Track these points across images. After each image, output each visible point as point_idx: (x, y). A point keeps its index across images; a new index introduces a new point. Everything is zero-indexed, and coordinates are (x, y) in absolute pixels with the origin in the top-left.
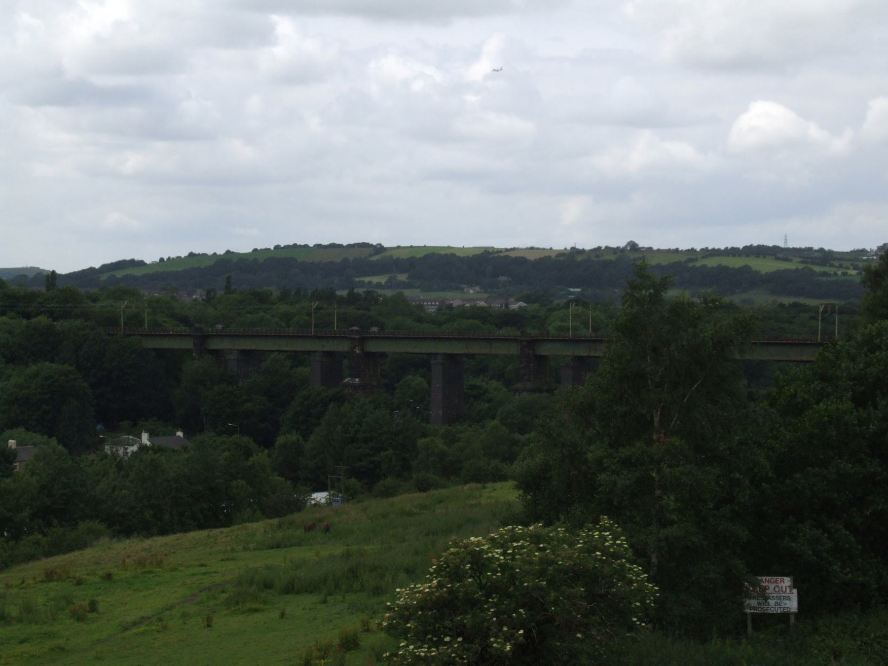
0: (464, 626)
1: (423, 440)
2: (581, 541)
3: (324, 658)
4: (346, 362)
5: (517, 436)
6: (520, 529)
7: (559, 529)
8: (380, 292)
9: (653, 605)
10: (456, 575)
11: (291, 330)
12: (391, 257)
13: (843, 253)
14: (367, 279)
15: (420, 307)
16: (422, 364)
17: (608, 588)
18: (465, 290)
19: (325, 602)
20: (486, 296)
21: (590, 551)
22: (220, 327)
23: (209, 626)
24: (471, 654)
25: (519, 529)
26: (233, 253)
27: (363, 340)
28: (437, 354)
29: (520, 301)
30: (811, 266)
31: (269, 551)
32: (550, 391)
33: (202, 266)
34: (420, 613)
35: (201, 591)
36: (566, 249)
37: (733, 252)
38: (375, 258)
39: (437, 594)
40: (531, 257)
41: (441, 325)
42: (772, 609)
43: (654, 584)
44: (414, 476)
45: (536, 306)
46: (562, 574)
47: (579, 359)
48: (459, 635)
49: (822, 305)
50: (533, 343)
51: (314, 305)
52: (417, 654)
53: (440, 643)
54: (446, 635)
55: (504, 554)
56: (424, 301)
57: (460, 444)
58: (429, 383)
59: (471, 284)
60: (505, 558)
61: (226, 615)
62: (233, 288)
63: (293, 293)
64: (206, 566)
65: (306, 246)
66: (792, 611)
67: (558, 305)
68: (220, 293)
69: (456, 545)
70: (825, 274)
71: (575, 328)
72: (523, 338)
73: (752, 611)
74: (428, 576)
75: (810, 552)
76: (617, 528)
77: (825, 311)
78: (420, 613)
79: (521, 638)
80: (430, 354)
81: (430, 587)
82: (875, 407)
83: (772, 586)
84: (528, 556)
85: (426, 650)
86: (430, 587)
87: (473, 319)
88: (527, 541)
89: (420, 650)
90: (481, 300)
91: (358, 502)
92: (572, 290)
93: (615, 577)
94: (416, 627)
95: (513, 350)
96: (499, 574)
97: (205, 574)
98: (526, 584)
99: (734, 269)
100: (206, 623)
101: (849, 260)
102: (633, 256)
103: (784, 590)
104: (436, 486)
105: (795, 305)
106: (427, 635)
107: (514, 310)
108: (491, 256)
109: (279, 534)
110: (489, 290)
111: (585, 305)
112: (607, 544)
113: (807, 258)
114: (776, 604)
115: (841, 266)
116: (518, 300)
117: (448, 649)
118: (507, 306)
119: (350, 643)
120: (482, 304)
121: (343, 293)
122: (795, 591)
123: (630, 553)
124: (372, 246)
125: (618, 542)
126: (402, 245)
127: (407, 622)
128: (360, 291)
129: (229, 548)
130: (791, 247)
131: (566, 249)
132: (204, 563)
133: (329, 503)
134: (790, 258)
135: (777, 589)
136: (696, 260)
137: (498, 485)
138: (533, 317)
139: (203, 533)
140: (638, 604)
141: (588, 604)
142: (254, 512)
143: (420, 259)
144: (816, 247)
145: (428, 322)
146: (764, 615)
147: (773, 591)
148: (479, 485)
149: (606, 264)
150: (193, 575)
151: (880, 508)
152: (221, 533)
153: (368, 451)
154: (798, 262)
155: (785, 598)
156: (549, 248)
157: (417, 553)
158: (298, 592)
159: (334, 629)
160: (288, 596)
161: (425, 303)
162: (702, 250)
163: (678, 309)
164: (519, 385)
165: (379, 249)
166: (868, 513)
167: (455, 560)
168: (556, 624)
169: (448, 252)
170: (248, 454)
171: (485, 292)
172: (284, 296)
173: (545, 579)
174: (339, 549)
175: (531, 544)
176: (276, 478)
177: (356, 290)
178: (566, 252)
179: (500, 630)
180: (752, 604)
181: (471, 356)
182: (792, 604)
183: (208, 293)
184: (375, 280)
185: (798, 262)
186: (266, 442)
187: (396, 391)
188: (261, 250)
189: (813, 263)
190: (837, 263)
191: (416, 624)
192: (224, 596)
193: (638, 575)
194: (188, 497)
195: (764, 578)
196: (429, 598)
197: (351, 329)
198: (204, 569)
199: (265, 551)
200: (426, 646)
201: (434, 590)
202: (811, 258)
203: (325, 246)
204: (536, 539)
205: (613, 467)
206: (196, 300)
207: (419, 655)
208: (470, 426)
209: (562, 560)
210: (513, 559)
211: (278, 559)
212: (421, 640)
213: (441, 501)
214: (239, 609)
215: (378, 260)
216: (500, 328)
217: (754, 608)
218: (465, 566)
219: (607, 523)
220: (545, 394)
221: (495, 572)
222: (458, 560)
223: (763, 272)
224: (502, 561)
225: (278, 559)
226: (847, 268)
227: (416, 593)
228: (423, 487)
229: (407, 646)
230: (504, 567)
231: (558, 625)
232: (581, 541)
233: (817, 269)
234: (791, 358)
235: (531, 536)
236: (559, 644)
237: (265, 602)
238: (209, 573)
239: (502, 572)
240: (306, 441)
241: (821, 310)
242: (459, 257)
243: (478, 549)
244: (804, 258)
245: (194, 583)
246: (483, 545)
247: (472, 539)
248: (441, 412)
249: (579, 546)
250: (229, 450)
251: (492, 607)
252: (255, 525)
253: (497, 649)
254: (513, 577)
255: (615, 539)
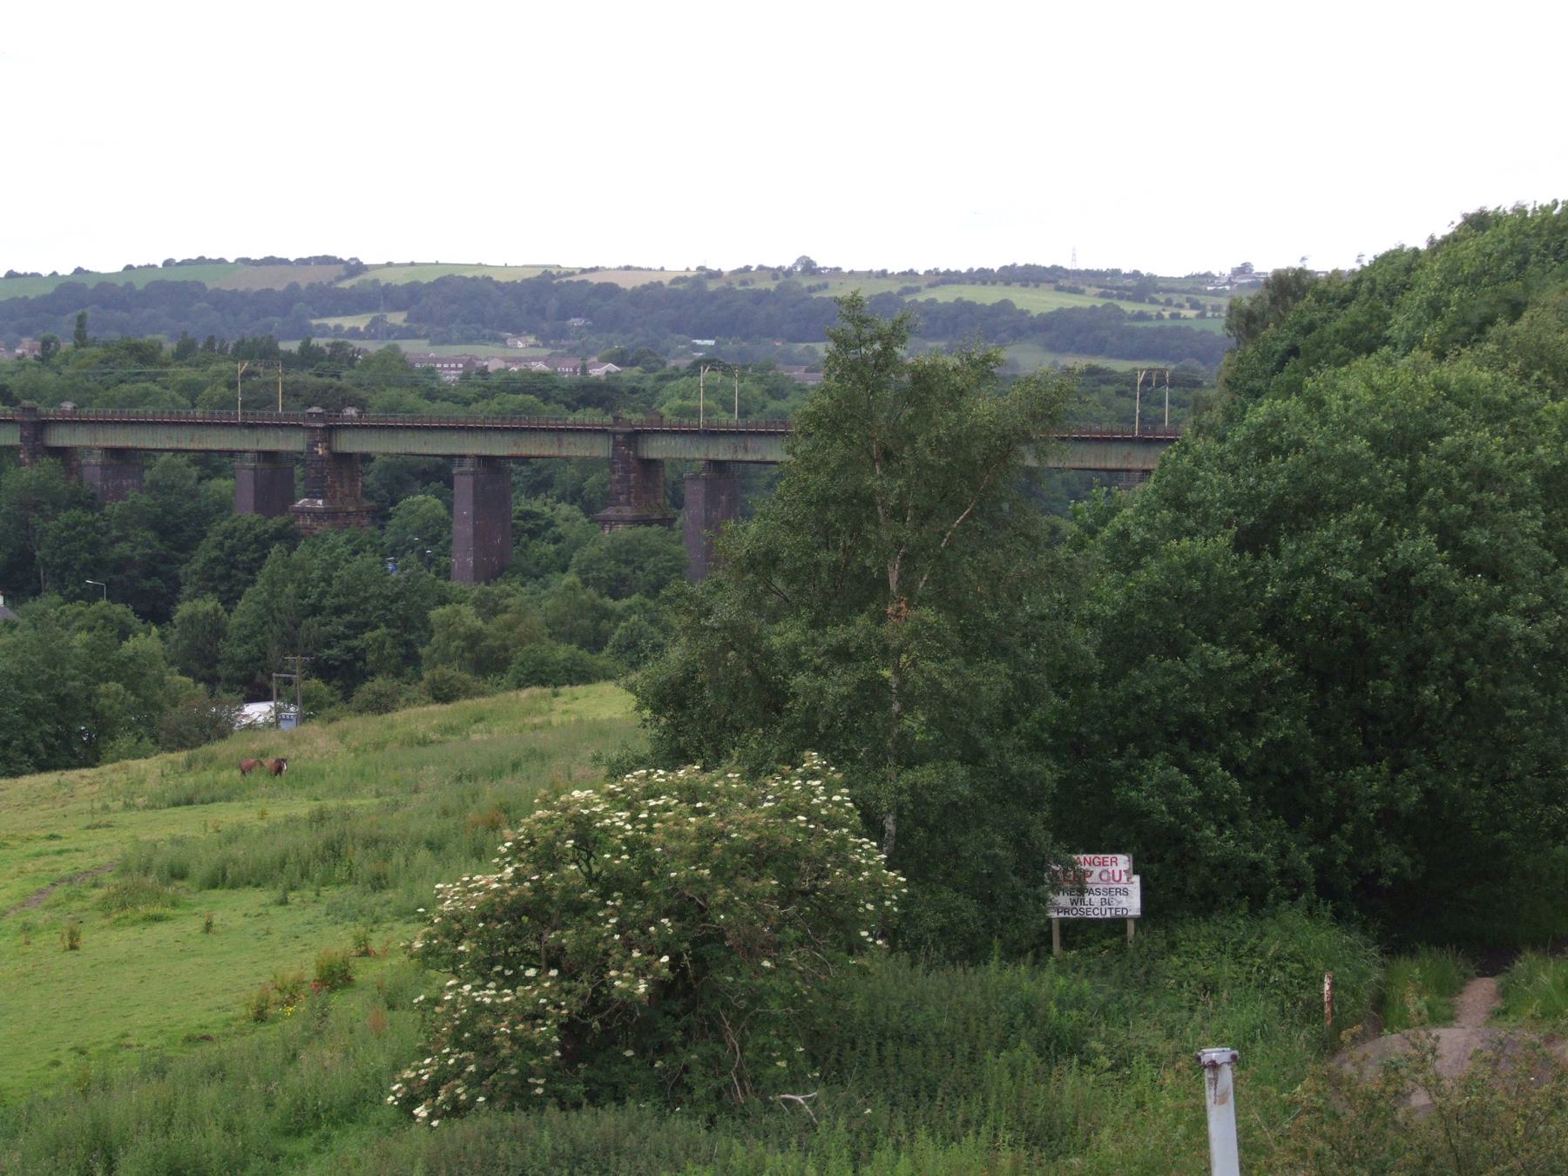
0: (562, 949)
1: (440, 610)
2: (770, 797)
3: (289, 1005)
4: (299, 471)
5: (609, 602)
6: (660, 776)
7: (730, 775)
8: (358, 344)
9: (895, 909)
10: (549, 858)
11: (199, 412)
12: (376, 281)
13: (1172, 279)
14: (332, 322)
15: (430, 371)
16: (438, 473)
17: (816, 879)
18: (509, 343)
19: (283, 902)
20: (546, 352)
21: (787, 814)
22: (68, 406)
23: (73, 947)
24: (574, 1000)
25: (659, 776)
26: (88, 272)
27: (331, 430)
28: (463, 457)
29: (608, 362)
30: (1116, 302)
31: (173, 810)
32: (667, 522)
33: (32, 296)
34: (481, 925)
35: (54, 885)
36: (688, 270)
37: (982, 277)
38: (346, 284)
39: (513, 893)
40: (627, 283)
41: (467, 404)
42: (1096, 911)
43: (898, 872)
44: (426, 675)
45: (636, 371)
46: (738, 856)
47: (717, 465)
48: (551, 965)
49: (1142, 371)
50: (635, 436)
51: (242, 368)
52: (478, 999)
53: (515, 981)
54: (528, 966)
55: (633, 820)
56: (437, 360)
57: (507, 616)
58: (449, 507)
59: (518, 331)
60: (634, 827)
61: (103, 927)
62: (90, 334)
63: (200, 346)
64: (60, 838)
65: (221, 261)
66: (1130, 913)
67: (676, 369)
68: (67, 345)
69: (546, 804)
70: (1141, 316)
71: (708, 412)
72: (617, 428)
73: (1062, 915)
74: (497, 860)
75: (1164, 808)
76: (834, 772)
77: (1146, 382)
78: (481, 925)
79: (665, 971)
80: (451, 457)
81: (500, 881)
82: (1276, 554)
83: (1097, 870)
84: (675, 824)
85: (493, 992)
86: (500, 881)
87: (525, 393)
88: (674, 798)
89: (481, 993)
90: (537, 359)
91: (332, 720)
92: (699, 342)
93: (830, 859)
94: (474, 951)
95: (601, 449)
96: (625, 857)
97: (60, 853)
98: (673, 874)
99: (983, 306)
100: (67, 944)
101: (1183, 292)
102: (807, 282)
103: (1117, 878)
104: (468, 693)
105: (1092, 371)
106: (493, 965)
107: (598, 378)
108: (555, 282)
109: (189, 780)
110: (552, 342)
111: (727, 370)
112: (815, 801)
113: (1111, 288)
114: (1103, 902)
115: (1169, 303)
116: (605, 360)
117: (533, 990)
118: (584, 370)
119: (335, 978)
120: (540, 366)
121: (293, 346)
122: (1136, 879)
123: (856, 818)
124: (341, 261)
125: (836, 798)
126: (396, 261)
127: (458, 943)
128: (320, 342)
129: (98, 805)
130: (1083, 268)
131: (688, 270)
132: (56, 832)
133: (275, 724)
134: (1081, 287)
135: (1105, 876)
136: (918, 290)
137: (580, 690)
138: (633, 391)
139: (50, 778)
140: (870, 907)
141: (781, 908)
142: (140, 740)
143: (429, 285)
144: (1126, 270)
145: (444, 400)
146: (1080, 921)
147: (1098, 880)
148: (548, 690)
149: (760, 297)
150: (39, 855)
151: (1280, 735)
152: (83, 777)
153: (341, 628)
154: (1095, 295)
155: (1118, 891)
156: (658, 267)
157: (446, 813)
158: (234, 886)
159: (302, 951)
160: (216, 893)
161: (439, 366)
162: (928, 272)
163: (924, 380)
164: (609, 512)
165: (355, 268)
166: (1260, 745)
167: (546, 831)
168: (727, 944)
169: (479, 274)
170: (124, 634)
171: (545, 346)
172: (185, 352)
173: (708, 865)
174: (302, 808)
175: (681, 802)
176: (178, 678)
177: (314, 342)
178: (689, 275)
179: (628, 957)
180: (1061, 905)
181: (524, 460)
182: (1132, 903)
183: (46, 344)
184: (348, 323)
185: (1095, 295)
186: (157, 613)
187: (390, 523)
188: (140, 267)
189: (1121, 297)
190: (1162, 298)
191: (474, 945)
192: (99, 893)
193: (870, 856)
194: (17, 713)
195: (1082, 857)
196: (498, 900)
197: (309, 410)
198: (56, 845)
199: (163, 811)
200: (492, 985)
201: (507, 885)
202: (1117, 288)
203: (255, 261)
204: (690, 793)
205: (818, 661)
206: (22, 356)
207: (481, 1002)
208: (523, 585)
209: (738, 829)
210: (650, 830)
211: (189, 824)
212: (483, 975)
213: (480, 719)
214: (127, 917)
215: (353, 287)
216: (574, 411)
217: (1065, 910)
218: (564, 843)
219: (816, 765)
220: (656, 528)
221: (617, 853)
222: (551, 833)
223: (1035, 313)
224: (630, 833)
225: (189, 824)
226: (1181, 306)
227: (471, 891)
228: (443, 694)
229: (460, 985)
230: (633, 845)
231: (731, 947)
232: (770, 797)
233: (1129, 307)
234: (1087, 465)
235: (680, 789)
236: (730, 979)
237: (174, 905)
238: (68, 851)
239: (631, 852)
240: (229, 611)
241: (1140, 380)
242: (498, 282)
243: (586, 812)
244: (1106, 287)
245: (39, 870)
246: (596, 805)
247: (576, 793)
248: (470, 560)
249: (766, 805)
250: (91, 629)
251: (612, 916)
252: (142, 764)
253: (622, 992)
254: (648, 863)
255: (829, 792)
